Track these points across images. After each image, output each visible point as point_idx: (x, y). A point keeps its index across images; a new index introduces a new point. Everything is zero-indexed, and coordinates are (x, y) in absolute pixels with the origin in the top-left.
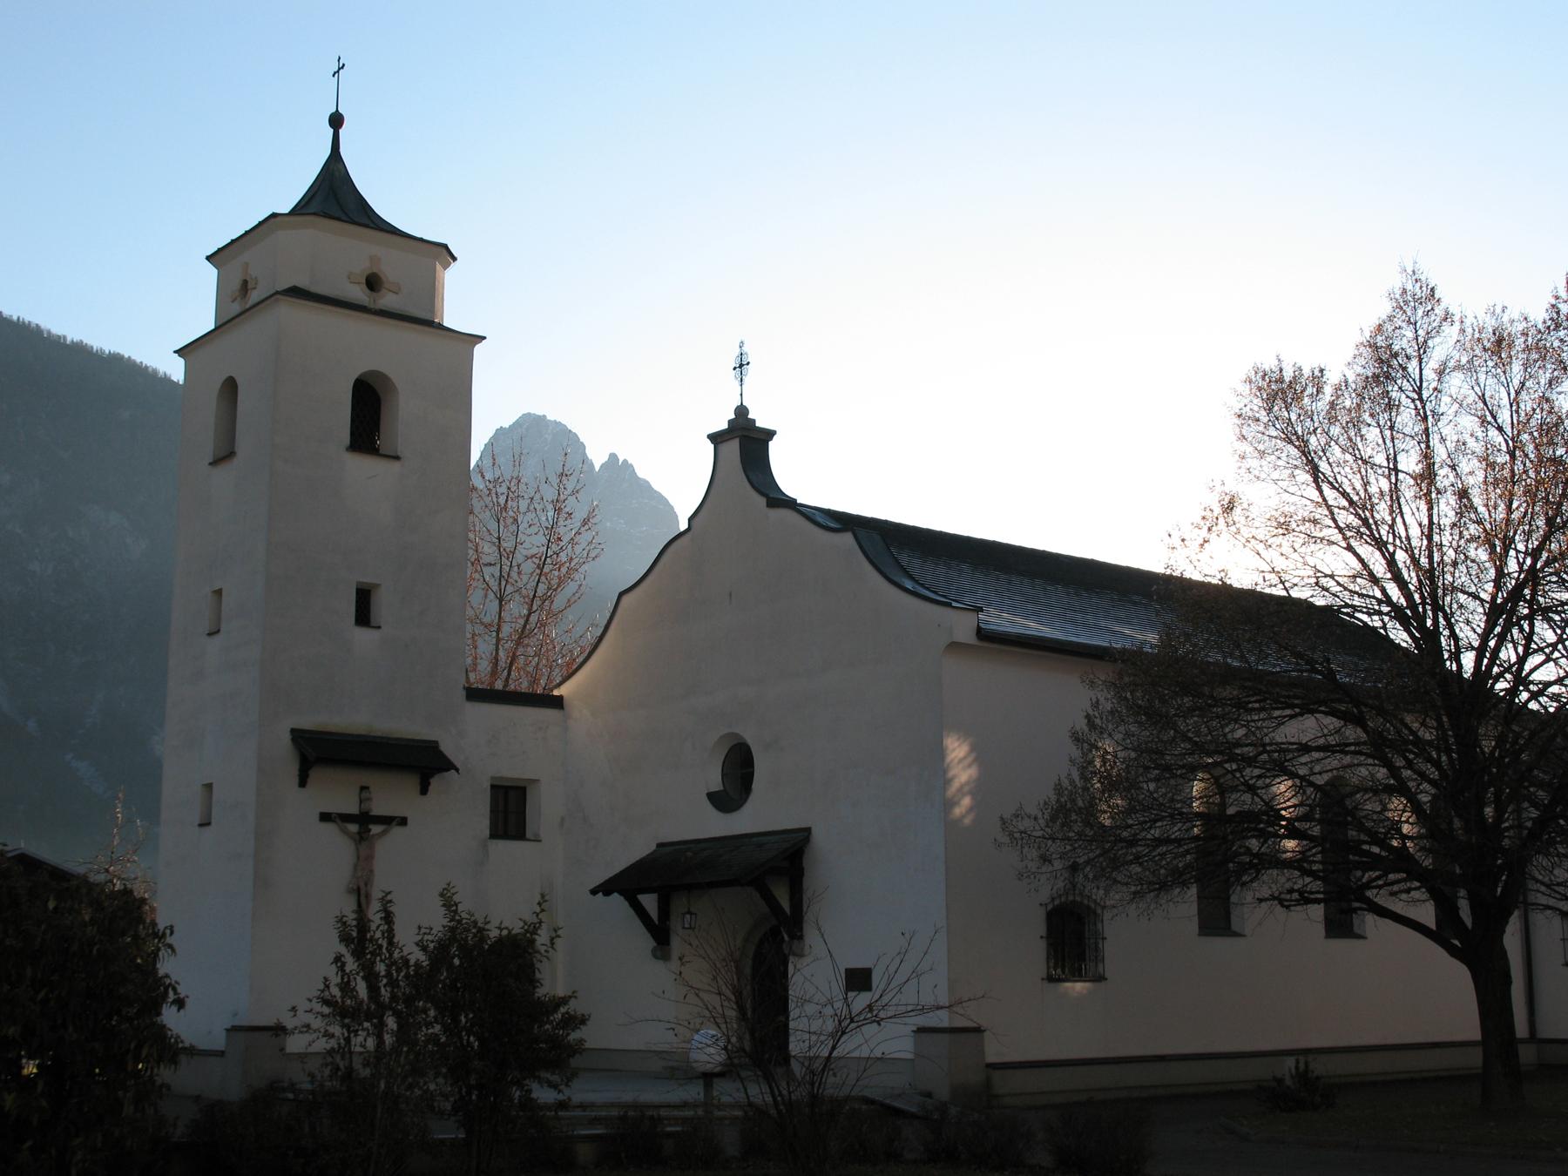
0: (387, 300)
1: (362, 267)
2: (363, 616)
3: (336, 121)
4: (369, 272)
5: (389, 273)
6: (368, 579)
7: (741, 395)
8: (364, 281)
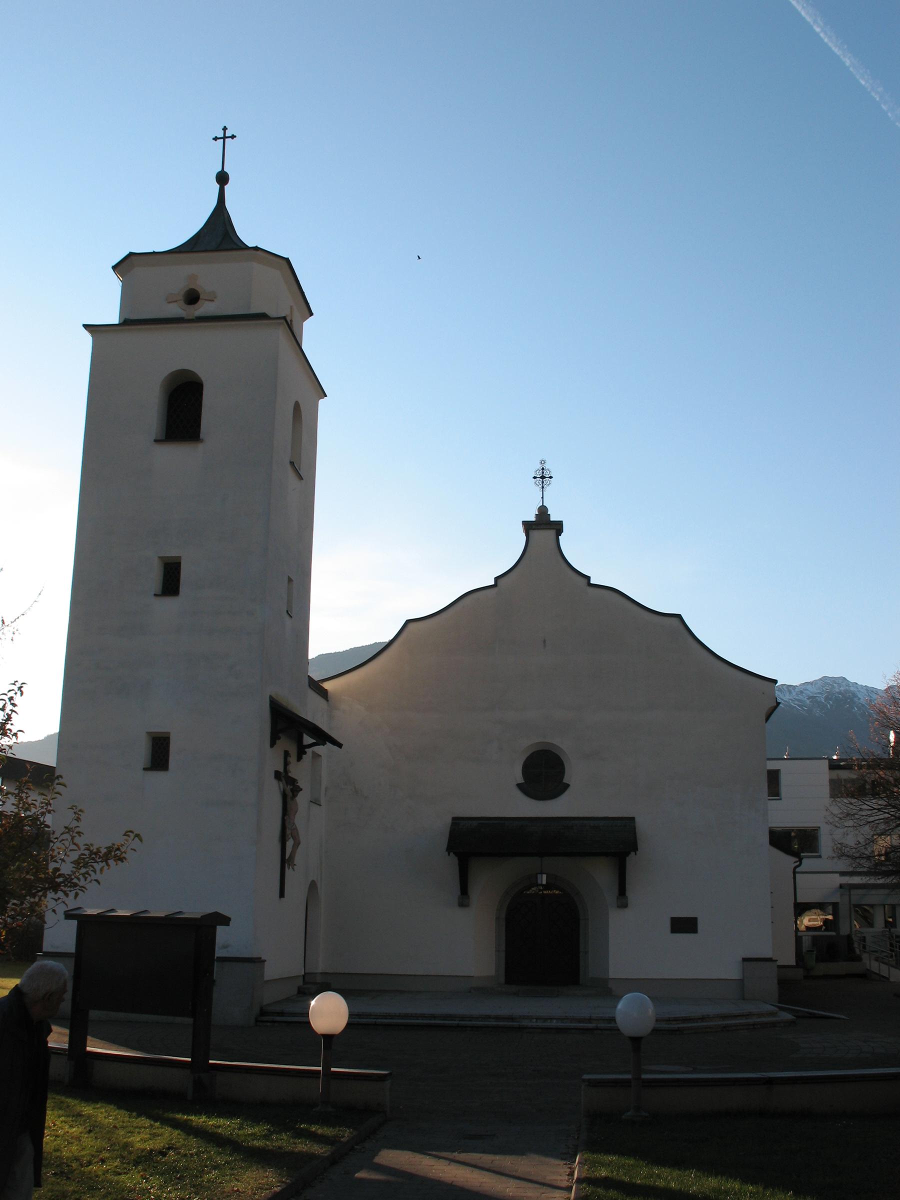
3: (222, 178)
7: (543, 498)
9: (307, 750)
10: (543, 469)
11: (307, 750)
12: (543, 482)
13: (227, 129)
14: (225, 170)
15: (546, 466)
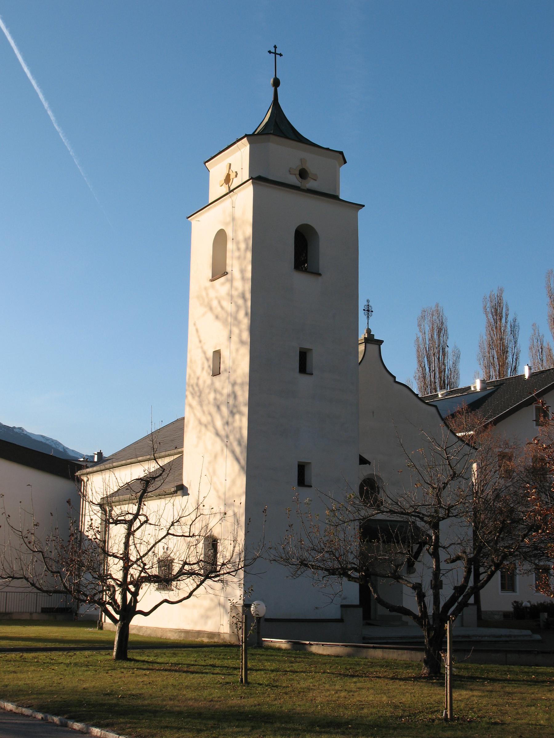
0: (311, 184)
1: (296, 165)
2: (303, 368)
3: (276, 83)
4: (301, 168)
5: (311, 168)
6: (307, 346)
7: (368, 323)
8: (298, 173)
9: (97, 453)
10: (368, 305)
11: (97, 453)
12: (368, 314)
13: (280, 56)
14: (277, 77)
15: (370, 304)
